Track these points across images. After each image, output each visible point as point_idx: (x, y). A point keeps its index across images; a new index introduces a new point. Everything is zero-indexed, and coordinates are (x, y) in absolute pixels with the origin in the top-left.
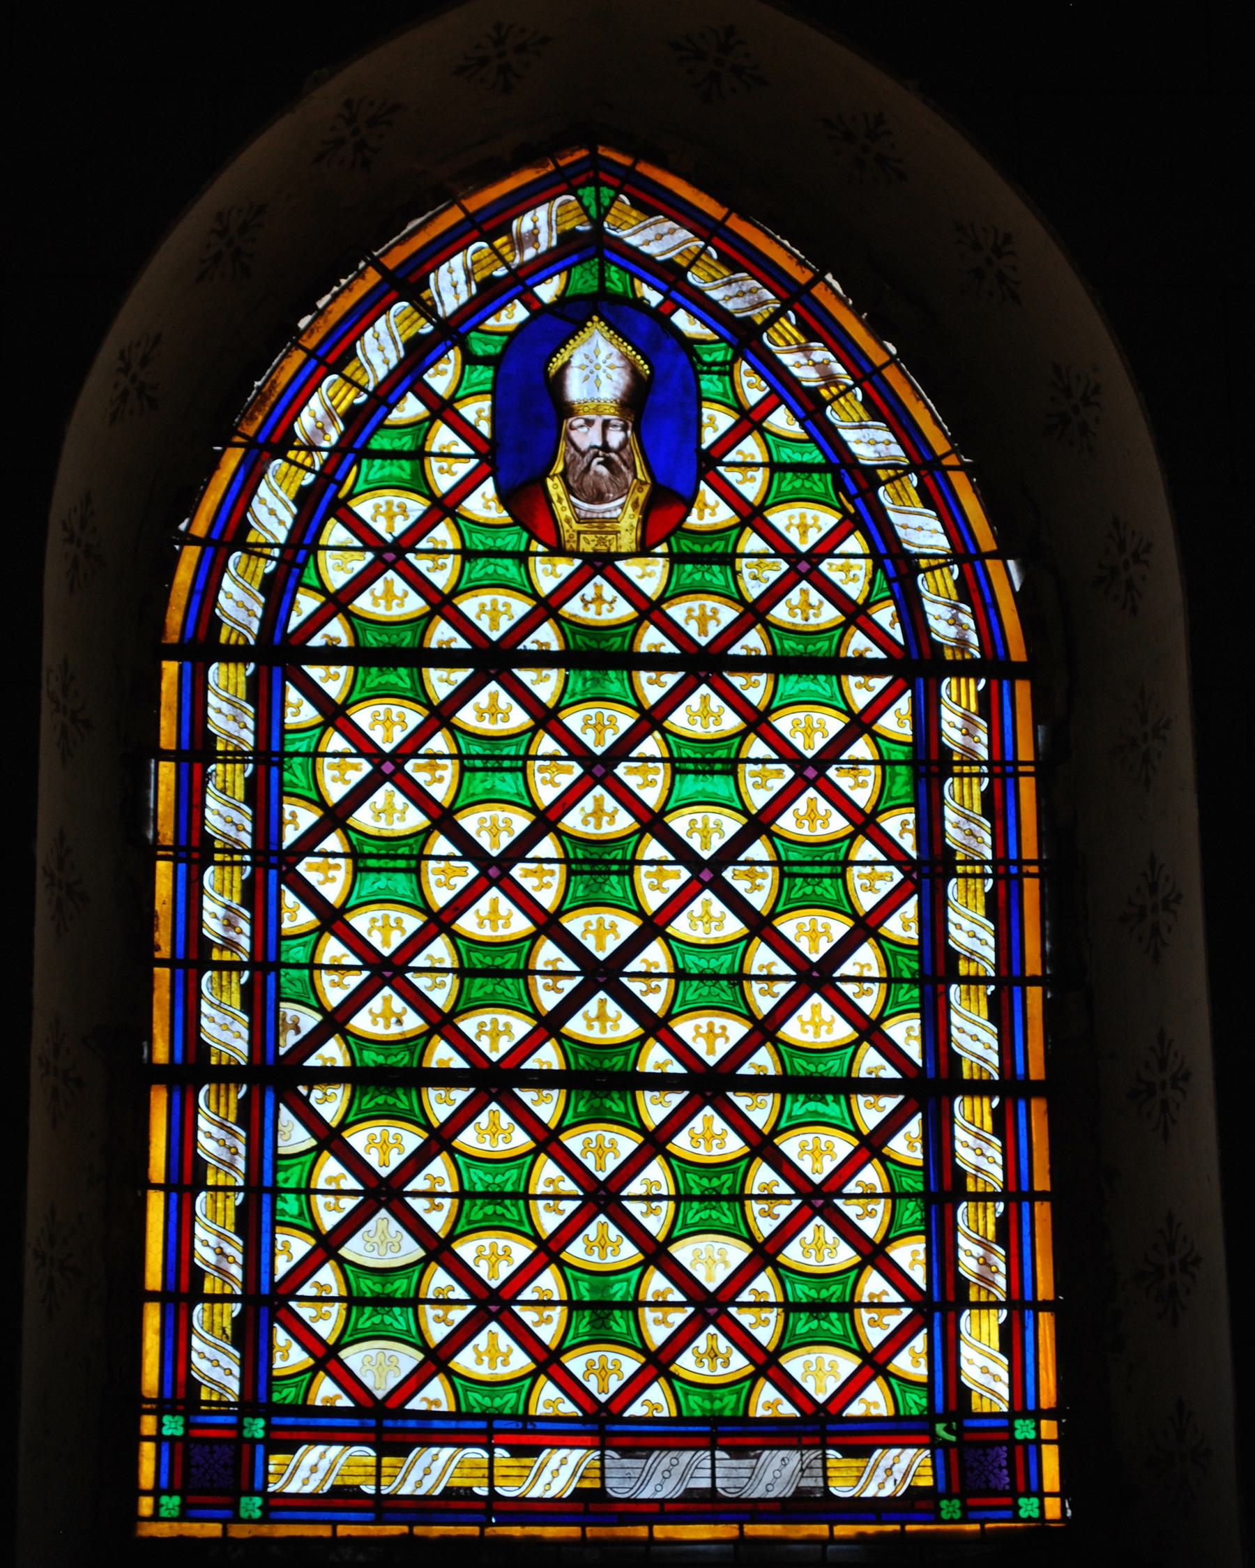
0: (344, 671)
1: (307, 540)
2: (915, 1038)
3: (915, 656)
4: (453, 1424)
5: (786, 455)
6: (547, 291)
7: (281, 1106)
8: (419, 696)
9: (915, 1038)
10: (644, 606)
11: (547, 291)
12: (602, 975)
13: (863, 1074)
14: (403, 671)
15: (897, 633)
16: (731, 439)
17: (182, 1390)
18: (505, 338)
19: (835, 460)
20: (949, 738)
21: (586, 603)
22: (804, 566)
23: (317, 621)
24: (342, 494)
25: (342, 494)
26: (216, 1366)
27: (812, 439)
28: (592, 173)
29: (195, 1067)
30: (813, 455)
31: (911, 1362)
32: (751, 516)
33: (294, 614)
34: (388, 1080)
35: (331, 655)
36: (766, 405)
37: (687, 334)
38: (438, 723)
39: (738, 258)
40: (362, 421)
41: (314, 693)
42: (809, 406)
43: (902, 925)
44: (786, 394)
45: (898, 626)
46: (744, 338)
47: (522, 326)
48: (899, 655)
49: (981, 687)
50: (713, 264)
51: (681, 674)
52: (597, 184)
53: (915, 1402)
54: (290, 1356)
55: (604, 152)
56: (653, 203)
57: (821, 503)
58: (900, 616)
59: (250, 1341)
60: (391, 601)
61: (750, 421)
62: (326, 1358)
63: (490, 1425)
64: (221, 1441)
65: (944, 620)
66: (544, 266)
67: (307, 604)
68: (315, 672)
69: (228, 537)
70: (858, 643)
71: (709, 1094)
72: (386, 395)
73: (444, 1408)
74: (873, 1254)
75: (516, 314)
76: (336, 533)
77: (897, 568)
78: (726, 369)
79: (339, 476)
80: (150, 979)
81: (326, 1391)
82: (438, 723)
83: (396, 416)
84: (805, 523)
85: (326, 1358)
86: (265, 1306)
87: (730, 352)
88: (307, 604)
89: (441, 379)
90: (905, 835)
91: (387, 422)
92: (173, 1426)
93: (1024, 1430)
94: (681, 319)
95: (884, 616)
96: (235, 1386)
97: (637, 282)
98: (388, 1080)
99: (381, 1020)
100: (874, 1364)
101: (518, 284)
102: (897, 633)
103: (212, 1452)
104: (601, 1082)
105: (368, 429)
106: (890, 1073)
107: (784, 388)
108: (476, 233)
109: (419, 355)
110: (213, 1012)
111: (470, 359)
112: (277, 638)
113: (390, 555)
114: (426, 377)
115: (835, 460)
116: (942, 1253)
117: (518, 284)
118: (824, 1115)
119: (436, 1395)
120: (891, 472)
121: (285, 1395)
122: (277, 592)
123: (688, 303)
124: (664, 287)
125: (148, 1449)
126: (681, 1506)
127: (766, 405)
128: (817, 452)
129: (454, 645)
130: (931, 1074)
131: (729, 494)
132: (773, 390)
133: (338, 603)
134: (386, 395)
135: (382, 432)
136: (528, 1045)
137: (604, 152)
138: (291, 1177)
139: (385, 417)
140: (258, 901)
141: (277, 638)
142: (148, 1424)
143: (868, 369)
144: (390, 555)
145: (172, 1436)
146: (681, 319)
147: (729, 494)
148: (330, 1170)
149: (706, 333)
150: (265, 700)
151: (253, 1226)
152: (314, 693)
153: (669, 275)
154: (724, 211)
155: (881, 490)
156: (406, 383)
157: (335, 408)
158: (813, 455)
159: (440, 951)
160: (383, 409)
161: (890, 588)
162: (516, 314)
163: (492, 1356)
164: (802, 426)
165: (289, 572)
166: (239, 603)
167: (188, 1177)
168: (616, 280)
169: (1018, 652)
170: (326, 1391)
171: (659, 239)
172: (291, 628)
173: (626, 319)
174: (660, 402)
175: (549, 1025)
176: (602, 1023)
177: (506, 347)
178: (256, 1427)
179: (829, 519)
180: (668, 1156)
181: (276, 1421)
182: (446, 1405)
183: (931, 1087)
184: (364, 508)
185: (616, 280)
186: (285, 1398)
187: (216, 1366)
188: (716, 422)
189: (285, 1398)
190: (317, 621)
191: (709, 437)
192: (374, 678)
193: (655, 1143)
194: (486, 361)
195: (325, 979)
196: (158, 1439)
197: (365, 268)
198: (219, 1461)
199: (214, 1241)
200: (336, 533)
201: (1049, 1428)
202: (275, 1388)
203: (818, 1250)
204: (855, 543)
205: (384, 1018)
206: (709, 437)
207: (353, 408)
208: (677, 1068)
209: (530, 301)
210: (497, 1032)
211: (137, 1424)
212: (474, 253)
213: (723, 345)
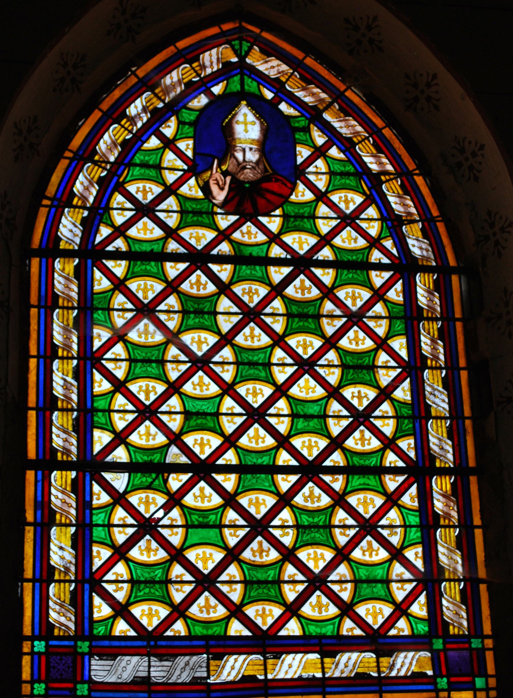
0: (124, 263)
1: (103, 205)
2: (412, 448)
3: (404, 262)
4: (187, 643)
5: (337, 168)
6: (217, 90)
7: (93, 482)
8: (163, 277)
9: (412, 448)
10: (272, 236)
11: (217, 90)
12: (256, 415)
13: (388, 465)
14: (153, 263)
15: (394, 251)
16: (310, 161)
17: (45, 629)
18: (198, 113)
19: (360, 170)
20: (421, 302)
21: (243, 234)
22: (348, 220)
23: (109, 239)
24: (121, 179)
25: (121, 179)
26: (61, 617)
27: (349, 161)
28: (240, 34)
29: (49, 461)
30: (350, 168)
31: (419, 608)
32: (321, 197)
33: (98, 235)
34: (150, 469)
35: (117, 255)
36: (327, 146)
37: (286, 114)
38: (172, 290)
39: (309, 78)
40: (130, 147)
41: (108, 274)
42: (348, 145)
43: (403, 393)
44: (335, 140)
45: (395, 249)
46: (314, 115)
47: (207, 106)
48: (397, 262)
49: (435, 277)
50: (298, 80)
51: (291, 268)
52: (241, 39)
53: (422, 628)
54: (102, 610)
55: (244, 24)
56: (269, 51)
57: (345, 206)
58: (395, 244)
59: (79, 604)
60: (145, 231)
61: (320, 152)
62: (121, 610)
63: (207, 643)
64: (65, 654)
65: (417, 247)
66: (215, 78)
67: (105, 231)
68: (110, 264)
69: (86, 155)
70: (376, 256)
71: (310, 476)
72: (141, 136)
73: (183, 634)
74: (397, 554)
75: (202, 101)
76: (118, 199)
77: (393, 223)
78: (306, 130)
79: (119, 172)
80: (25, 419)
81: (121, 627)
82: (172, 290)
83: (146, 146)
84: (349, 200)
85: (121, 610)
86: (88, 581)
87: (307, 122)
88: (105, 231)
89: (169, 130)
90: (267, 549)
91: (142, 148)
92: (40, 646)
93: (476, 643)
94: (283, 107)
95: (388, 244)
96: (72, 626)
97: (261, 87)
98: (150, 469)
99: (203, 340)
100: (401, 610)
101: (203, 85)
102: (394, 251)
103: (61, 659)
104: (256, 470)
105: (134, 151)
106: (401, 464)
107: (334, 137)
108: (182, 60)
109: (158, 118)
110: (59, 432)
111: (180, 123)
112: (90, 247)
113: (145, 210)
114: (161, 129)
115: (360, 170)
116: (430, 554)
117: (203, 85)
118: (368, 485)
119: (179, 627)
120: (387, 177)
121: (100, 630)
122: (89, 226)
123: (286, 99)
124: (275, 91)
125: (26, 660)
126: (430, 512)
127: (327, 146)
128: (351, 167)
129: (179, 251)
130: (420, 464)
131: (311, 187)
132: (330, 139)
133: (120, 231)
134: (141, 136)
135: (140, 152)
136: (219, 452)
137: (244, 24)
138: (99, 518)
139: (142, 145)
140: (82, 377)
141: (90, 247)
142: (26, 647)
143: (375, 129)
144: (145, 210)
145: (39, 652)
146: (283, 107)
147: (311, 187)
148: (120, 514)
149: (296, 113)
150: (83, 277)
151: (82, 543)
152: (108, 274)
153: (276, 85)
154: (27, 528)
155: (383, 186)
156: (151, 131)
157: (117, 140)
158: (350, 168)
159: (174, 402)
160: (140, 143)
161: (390, 232)
162: (202, 101)
163: (207, 608)
164: (344, 154)
165: (136, 143)
166: (69, 229)
167: (47, 518)
168: (251, 86)
169: (452, 262)
170: (121, 627)
171: (272, 67)
172: (97, 242)
173: (258, 105)
174: (278, 137)
175: (230, 441)
176: (257, 439)
177: (198, 117)
178: (84, 647)
179: (359, 199)
180: (292, 507)
181: (94, 643)
182: (183, 632)
183: (420, 470)
184: (132, 188)
185: (251, 86)
186: (100, 632)
187: (61, 617)
188: (303, 153)
189: (100, 632)
190: (109, 239)
191: (300, 160)
192: (139, 267)
193: (285, 500)
194: (190, 124)
195: (116, 416)
196: (32, 653)
197: (130, 75)
198: (65, 663)
199: (61, 552)
200: (118, 199)
201: (489, 643)
202: (95, 627)
203: (370, 553)
204: (372, 212)
205: (148, 436)
206: (300, 160)
207: (125, 141)
208: (294, 462)
209: (209, 93)
210: (203, 443)
211: (21, 647)
212: (182, 70)
213: (303, 118)
